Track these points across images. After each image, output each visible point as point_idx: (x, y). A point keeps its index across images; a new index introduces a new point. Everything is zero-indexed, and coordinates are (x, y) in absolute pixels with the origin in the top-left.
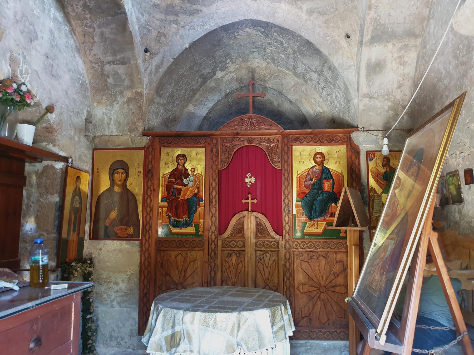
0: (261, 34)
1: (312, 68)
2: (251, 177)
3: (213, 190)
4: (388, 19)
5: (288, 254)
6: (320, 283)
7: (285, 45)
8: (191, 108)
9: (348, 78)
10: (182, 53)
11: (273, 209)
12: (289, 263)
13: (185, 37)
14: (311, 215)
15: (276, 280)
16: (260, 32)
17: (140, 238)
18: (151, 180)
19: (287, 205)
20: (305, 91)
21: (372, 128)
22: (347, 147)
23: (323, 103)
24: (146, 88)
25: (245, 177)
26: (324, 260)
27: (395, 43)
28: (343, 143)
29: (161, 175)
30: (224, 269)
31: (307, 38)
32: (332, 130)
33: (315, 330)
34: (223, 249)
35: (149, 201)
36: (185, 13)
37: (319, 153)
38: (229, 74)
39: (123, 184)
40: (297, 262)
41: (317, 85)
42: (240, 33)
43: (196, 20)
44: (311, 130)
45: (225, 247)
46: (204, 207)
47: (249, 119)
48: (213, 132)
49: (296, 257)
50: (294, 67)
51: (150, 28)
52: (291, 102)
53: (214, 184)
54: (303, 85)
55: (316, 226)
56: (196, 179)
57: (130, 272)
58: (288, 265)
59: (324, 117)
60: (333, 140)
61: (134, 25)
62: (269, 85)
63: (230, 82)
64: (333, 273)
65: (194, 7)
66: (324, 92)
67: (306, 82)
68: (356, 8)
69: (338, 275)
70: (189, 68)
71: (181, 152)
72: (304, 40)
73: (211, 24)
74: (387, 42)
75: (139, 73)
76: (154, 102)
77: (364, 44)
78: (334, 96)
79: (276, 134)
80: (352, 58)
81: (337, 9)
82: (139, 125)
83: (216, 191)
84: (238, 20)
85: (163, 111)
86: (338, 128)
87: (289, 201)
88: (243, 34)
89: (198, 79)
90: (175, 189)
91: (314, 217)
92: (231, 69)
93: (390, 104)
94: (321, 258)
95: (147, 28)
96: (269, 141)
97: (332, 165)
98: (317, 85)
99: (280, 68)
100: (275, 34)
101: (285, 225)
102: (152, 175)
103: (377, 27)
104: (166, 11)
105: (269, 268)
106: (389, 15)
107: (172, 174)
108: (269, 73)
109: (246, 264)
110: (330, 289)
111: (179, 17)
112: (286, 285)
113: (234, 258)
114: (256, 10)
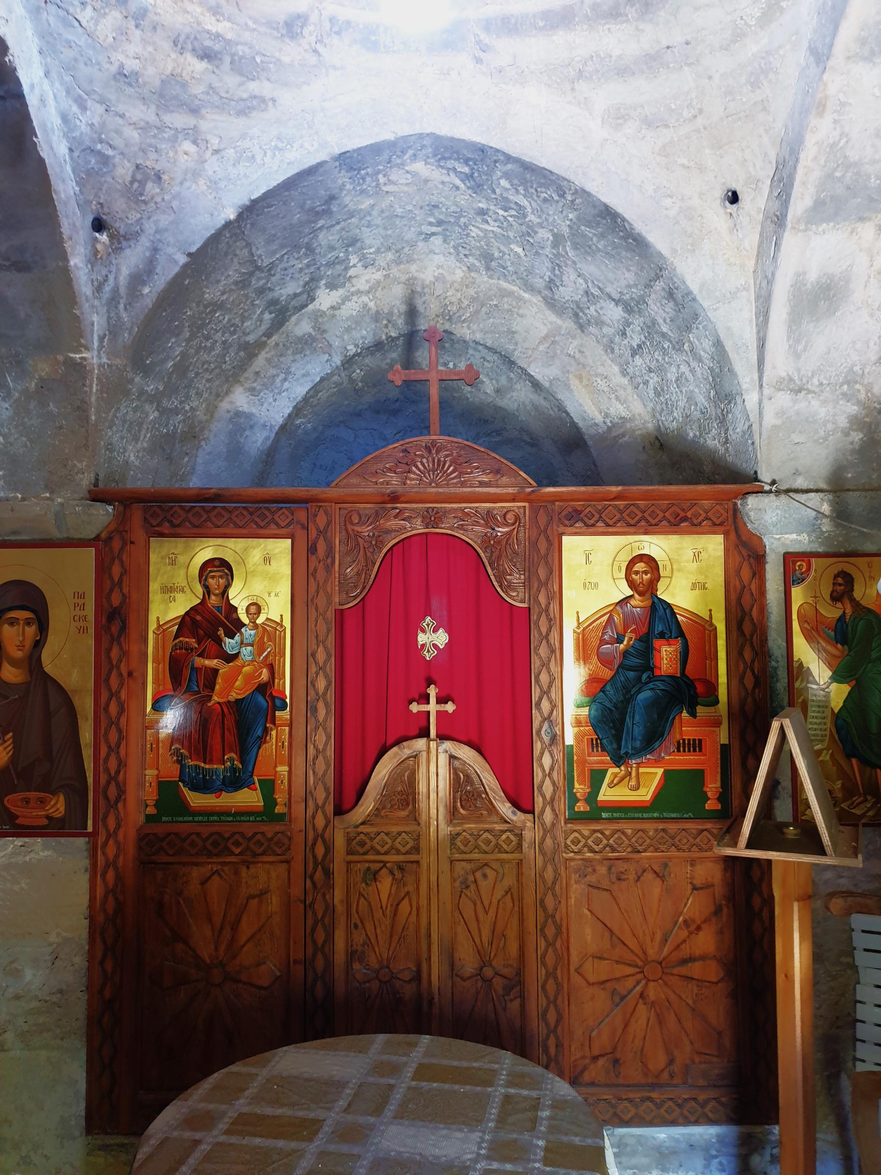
0: (458, 182)
1: (609, 289)
2: (435, 631)
3: (317, 674)
5: (550, 869)
6: (645, 953)
7: (531, 218)
8: (240, 399)
9: (729, 329)
11: (501, 725)
12: (554, 895)
13: (222, 184)
14: (619, 748)
15: (513, 948)
17: (90, 829)
18: (119, 644)
19: (548, 718)
20: (577, 355)
21: (800, 482)
22: (726, 539)
23: (630, 389)
24: (101, 347)
25: (412, 630)
26: (658, 882)
28: (714, 527)
29: (152, 626)
30: (355, 918)
31: (604, 199)
32: (685, 488)
33: (631, 1096)
34: (350, 858)
35: (113, 708)
37: (641, 558)
38: (355, 298)
39: (30, 657)
40: (577, 890)
42: (393, 177)
44: (620, 488)
45: (358, 853)
46: (291, 726)
47: (430, 452)
48: (315, 491)
49: (574, 877)
50: (551, 285)
51: (110, 152)
52: (536, 385)
53: (321, 656)
54: (574, 337)
55: (633, 783)
56: (262, 638)
57: (58, 934)
58: (550, 902)
59: (634, 431)
60: (685, 519)
62: (474, 332)
63: (357, 321)
64: (685, 921)
65: (253, 87)
66: (638, 360)
67: (581, 327)
68: (765, 109)
69: (699, 928)
70: (236, 283)
71: (216, 551)
72: (594, 206)
73: (307, 145)
74: (861, 219)
76: (127, 393)
77: (789, 225)
78: (672, 375)
79: (514, 500)
81: (701, 111)
82: (79, 465)
83: (326, 676)
84: (391, 137)
85: (156, 414)
86: (685, 477)
87: (553, 706)
88: (403, 181)
89: (262, 313)
90: (196, 670)
91: (627, 753)
92: (361, 284)
93: (853, 409)
94: (649, 876)
96: (489, 518)
97: (679, 594)
98: (617, 339)
99: (504, 284)
100: (504, 183)
101: (543, 782)
102: (124, 628)
103: (835, 170)
104: (161, 96)
105: (492, 912)
107: (189, 622)
108: (473, 299)
109: (423, 902)
110: (675, 971)
111: (202, 117)
112: (544, 964)
113: (385, 884)
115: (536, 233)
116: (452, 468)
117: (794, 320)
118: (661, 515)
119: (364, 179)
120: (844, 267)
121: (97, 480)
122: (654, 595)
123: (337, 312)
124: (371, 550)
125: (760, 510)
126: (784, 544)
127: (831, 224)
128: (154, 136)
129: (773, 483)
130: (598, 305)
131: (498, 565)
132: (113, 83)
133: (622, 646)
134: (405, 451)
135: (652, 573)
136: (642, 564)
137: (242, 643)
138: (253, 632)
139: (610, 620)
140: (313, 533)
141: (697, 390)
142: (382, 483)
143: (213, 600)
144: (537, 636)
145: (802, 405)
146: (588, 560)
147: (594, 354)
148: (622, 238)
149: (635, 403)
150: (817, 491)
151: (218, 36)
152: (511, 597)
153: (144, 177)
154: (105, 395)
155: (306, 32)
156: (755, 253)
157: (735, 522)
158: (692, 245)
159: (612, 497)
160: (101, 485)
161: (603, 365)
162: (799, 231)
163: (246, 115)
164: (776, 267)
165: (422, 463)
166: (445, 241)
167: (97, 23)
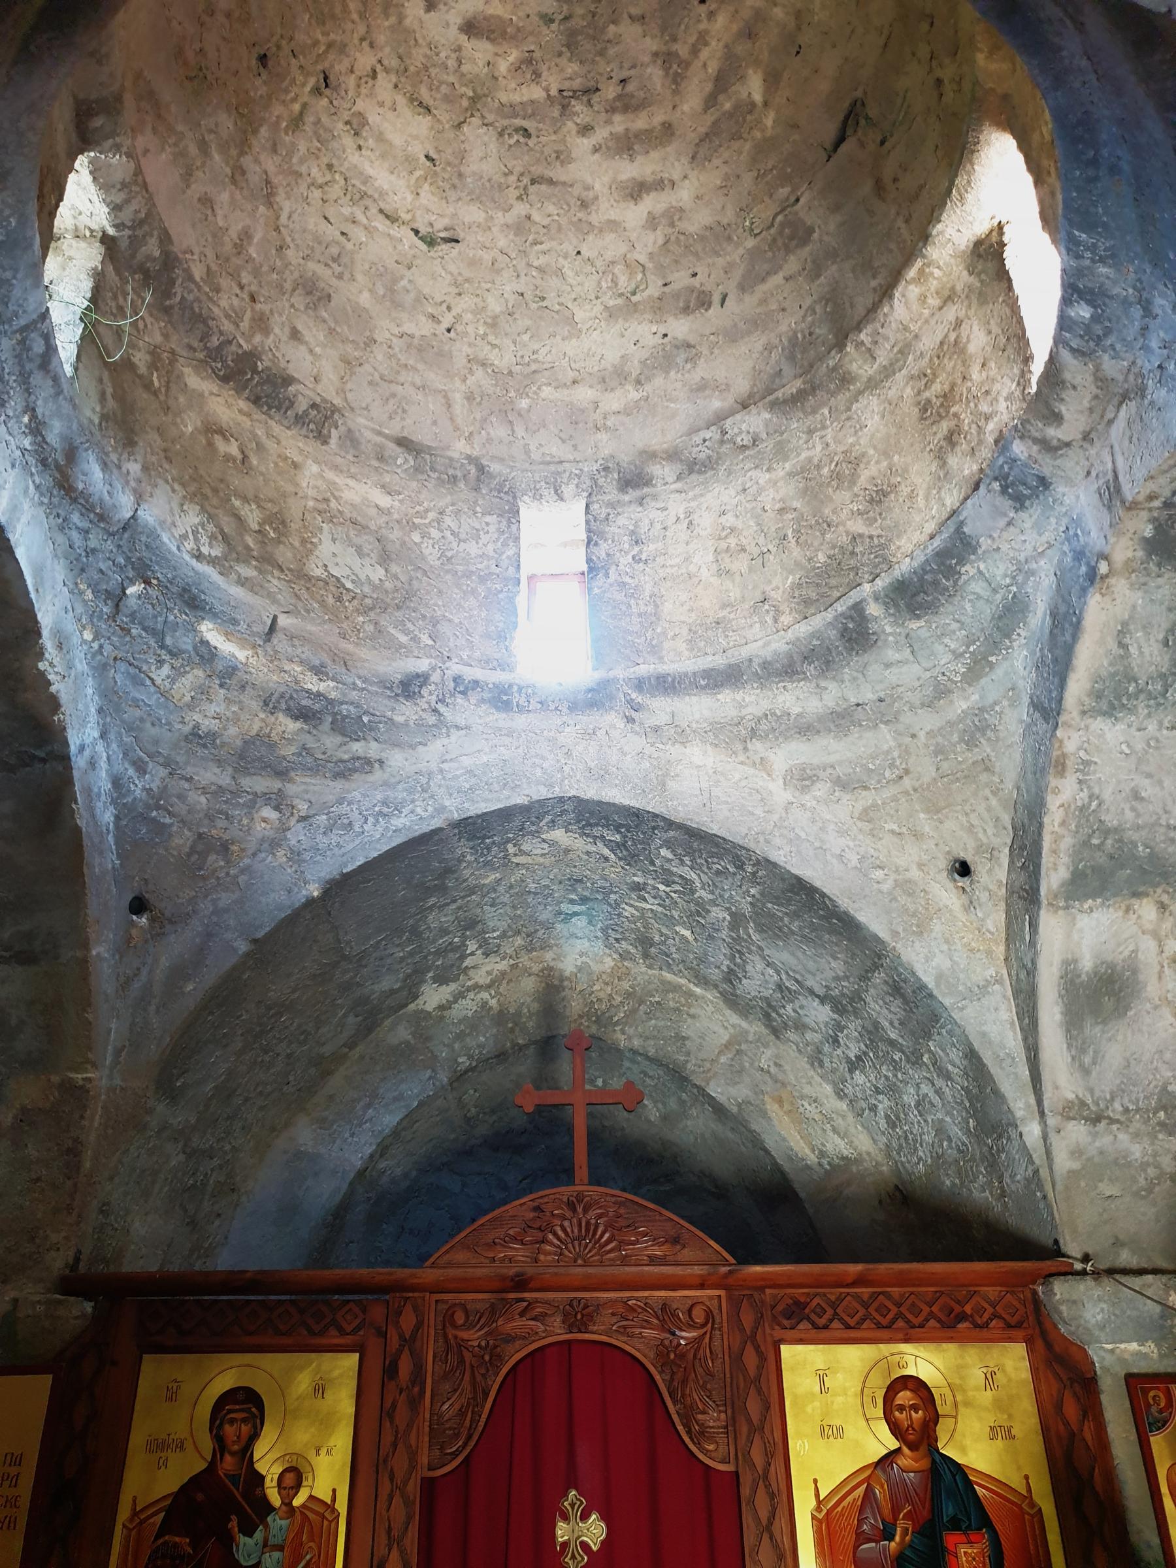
0: (606, 852)
1: (810, 983)
2: (585, 1517)
4: (1133, 809)
7: (701, 893)
8: (304, 1134)
9: (984, 1034)
10: (295, 916)
13: (307, 856)
16: (607, 843)
20: (773, 1070)
21: (1126, 1258)
22: (1031, 1350)
23: (851, 1118)
27: (1165, 898)
31: (795, 871)
36: (316, 769)
38: (471, 995)
41: (827, 1048)
43: (362, 793)
44: (859, 1267)
47: (574, 1210)
48: (401, 1273)
50: (730, 977)
51: (168, 820)
52: (719, 1110)
54: (766, 1046)
56: (299, 1533)
60: (963, 1317)
61: (100, 805)
62: (630, 1038)
63: (473, 1024)
65: (357, 747)
66: (859, 1078)
67: (776, 1032)
72: (783, 880)
73: (419, 810)
74: (1136, 895)
75: (86, 1001)
77: (1044, 902)
78: (909, 1098)
79: (702, 1286)
80: (989, 953)
81: (907, 772)
82: (54, 1238)
85: (182, 1157)
88: (539, 851)
89: (345, 1016)
95: (154, 820)
96: (667, 1316)
97: (973, 1447)
98: (827, 1048)
99: (669, 976)
100: (664, 852)
103: (1090, 836)
106: (1136, 795)
108: (628, 995)
111: (291, 781)
114: (592, 765)
115: (708, 911)
116: (607, 1235)
117: (1073, 1022)
118: (926, 1310)
119: (489, 849)
120: (1126, 953)
121: (77, 1260)
122: (933, 1449)
123: (446, 1013)
124: (483, 1371)
125: (1074, 1302)
126: (1122, 1361)
127: (1099, 900)
128: (226, 802)
129: (1086, 1258)
130: (797, 1003)
131: (683, 1396)
132: (183, 744)
133: (893, 1544)
134: (538, 1209)
135: (926, 1410)
136: (908, 1393)
137: (265, 1545)
138: (284, 1523)
139: (869, 1494)
140: (394, 1341)
141: (948, 1119)
142: (502, 1260)
143: (229, 1463)
144: (752, 1525)
145: (1105, 1141)
146: (823, 1389)
147: (796, 1067)
148: (821, 918)
149: (861, 1137)
150: (1155, 1271)
151: (319, 694)
152: (706, 1452)
153: (210, 847)
154: (110, 1131)
155: (425, 692)
156: (1003, 935)
157: (1040, 1323)
158: (918, 926)
159: (850, 1281)
160: (82, 1268)
161: (810, 1083)
162: (1059, 908)
163: (344, 777)
164: (1036, 953)
165: (562, 1226)
166: (590, 922)
167: (173, 682)
